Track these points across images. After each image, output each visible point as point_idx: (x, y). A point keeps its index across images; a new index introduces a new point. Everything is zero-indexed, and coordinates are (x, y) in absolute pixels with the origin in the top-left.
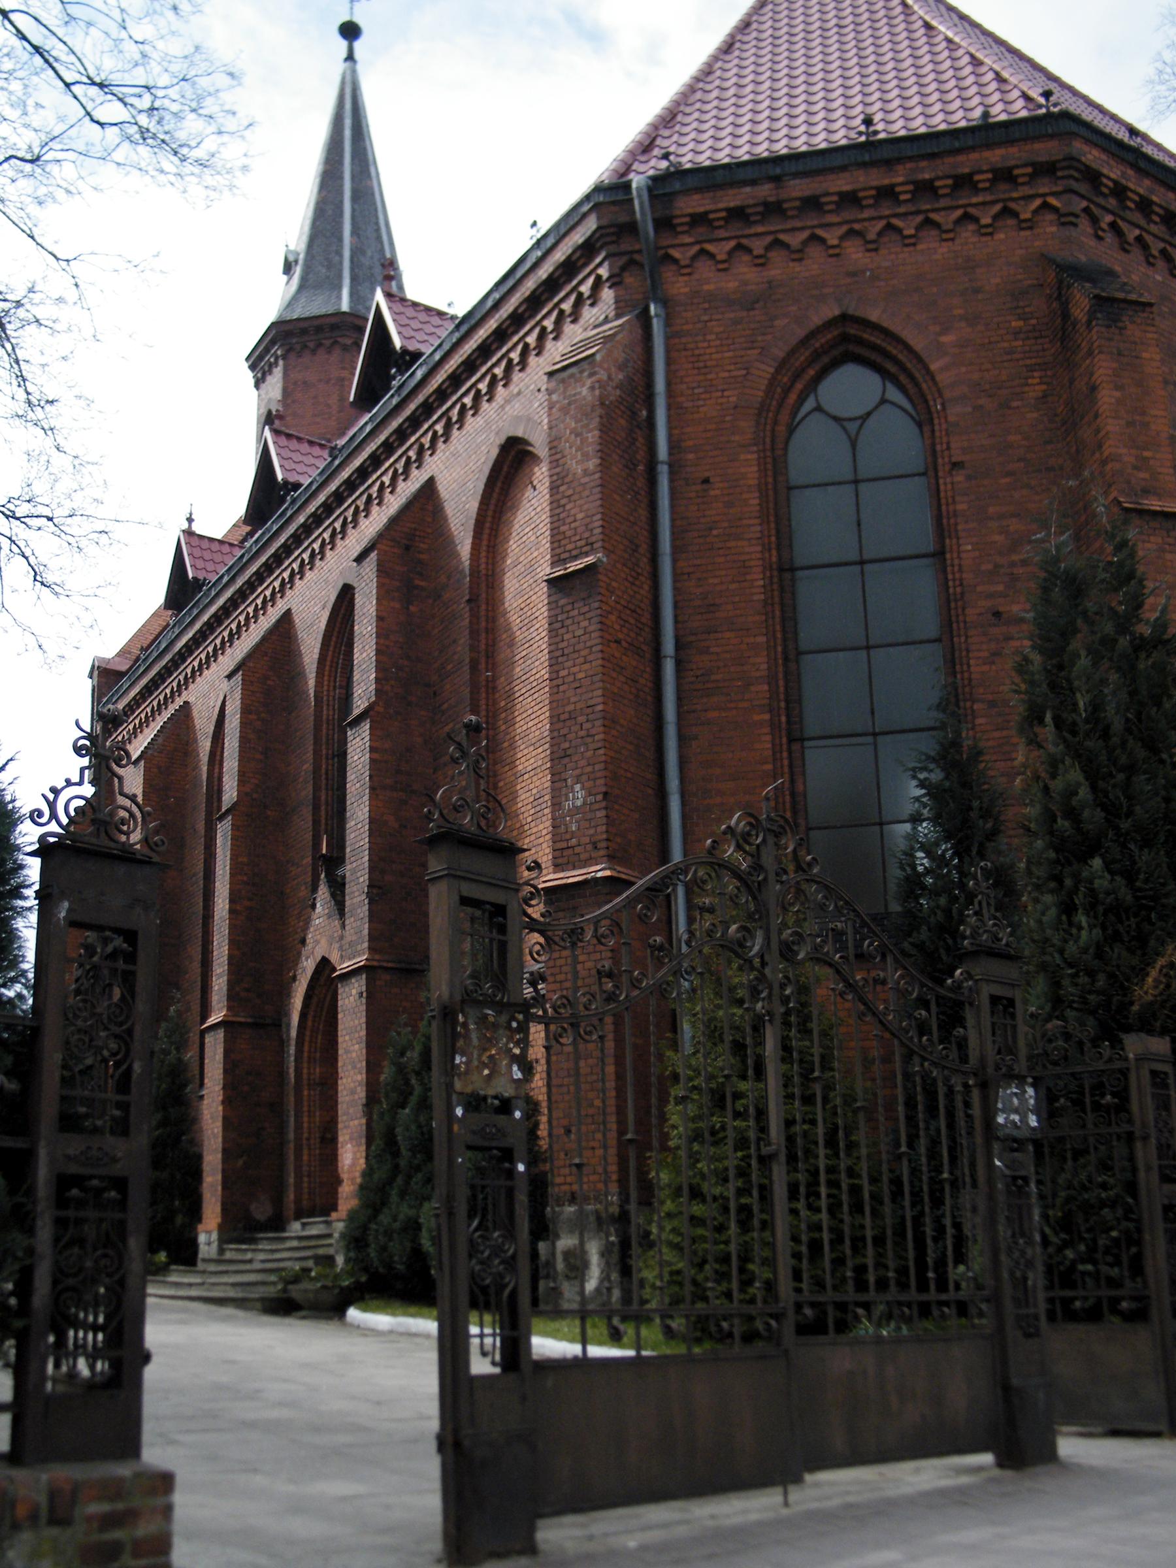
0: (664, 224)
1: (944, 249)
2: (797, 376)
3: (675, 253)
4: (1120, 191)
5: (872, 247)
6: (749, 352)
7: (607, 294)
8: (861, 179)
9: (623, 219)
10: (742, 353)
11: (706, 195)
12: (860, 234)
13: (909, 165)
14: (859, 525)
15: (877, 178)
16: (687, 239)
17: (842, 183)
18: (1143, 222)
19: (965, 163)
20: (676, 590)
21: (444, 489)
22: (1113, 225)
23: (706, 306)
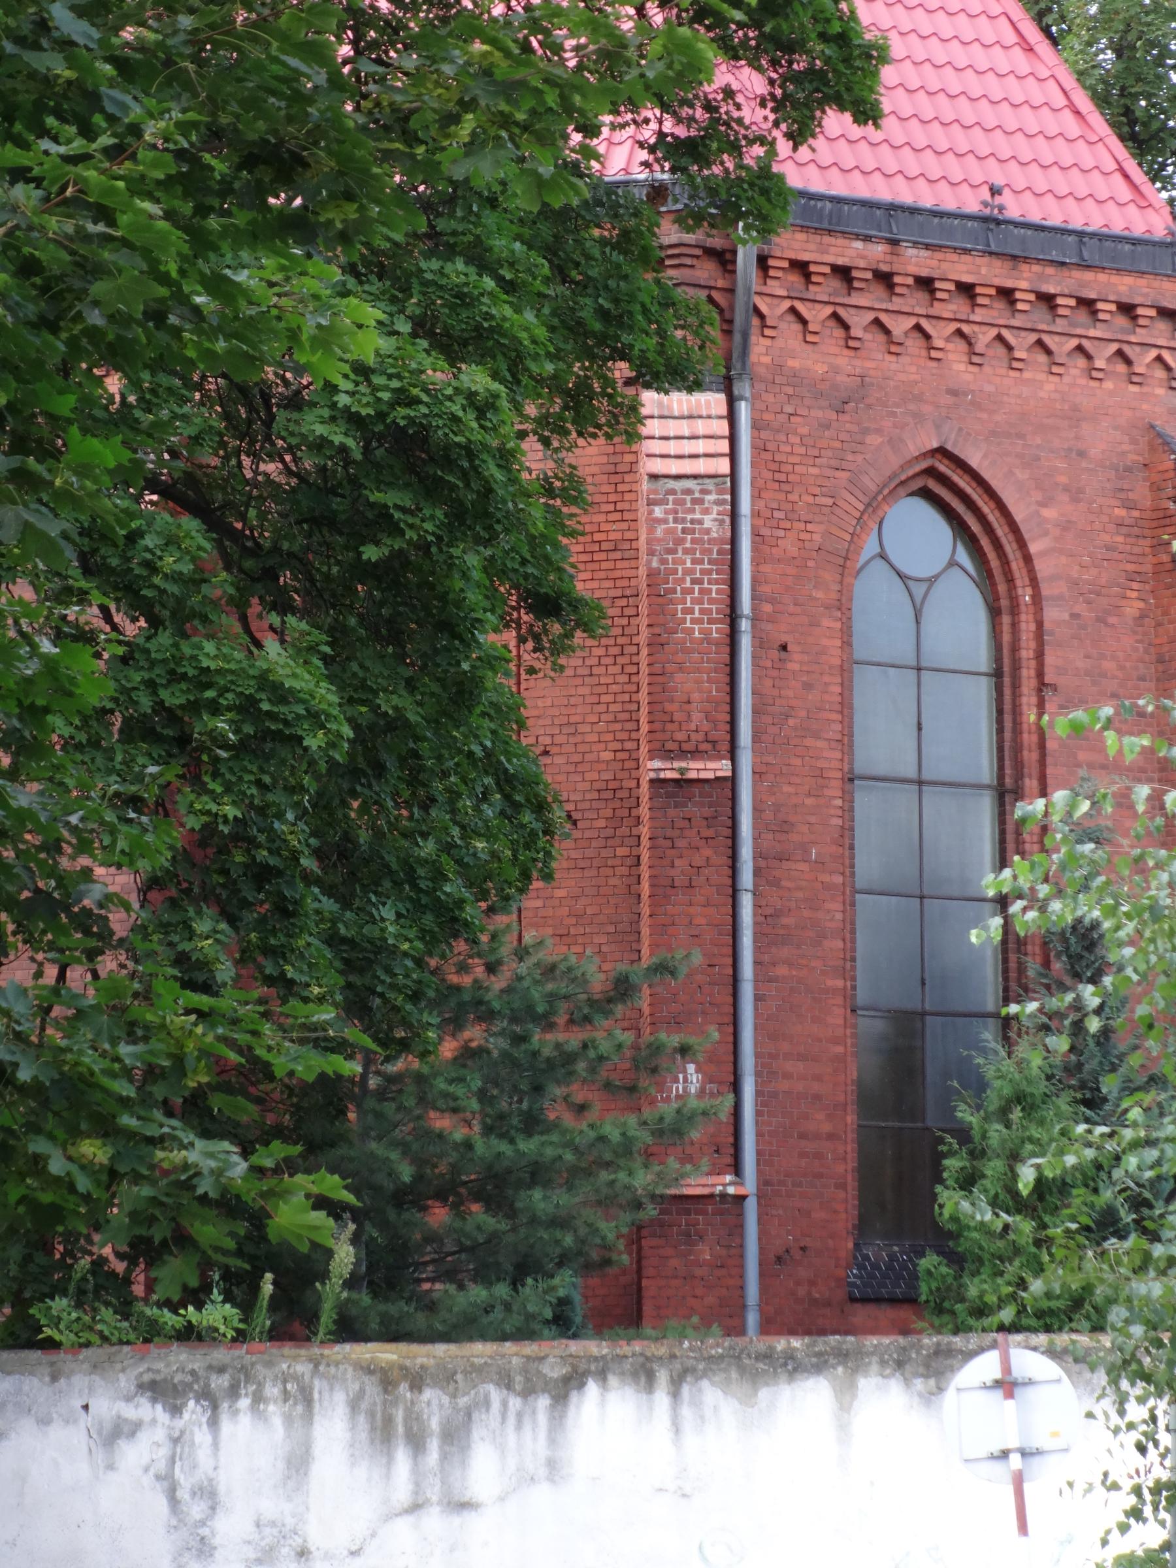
1: (1050, 385)
6: (838, 474)
8: (984, 271)
10: (830, 473)
11: (812, 237)
13: (1036, 268)
14: (920, 728)
19: (1093, 284)
23: (790, 390)
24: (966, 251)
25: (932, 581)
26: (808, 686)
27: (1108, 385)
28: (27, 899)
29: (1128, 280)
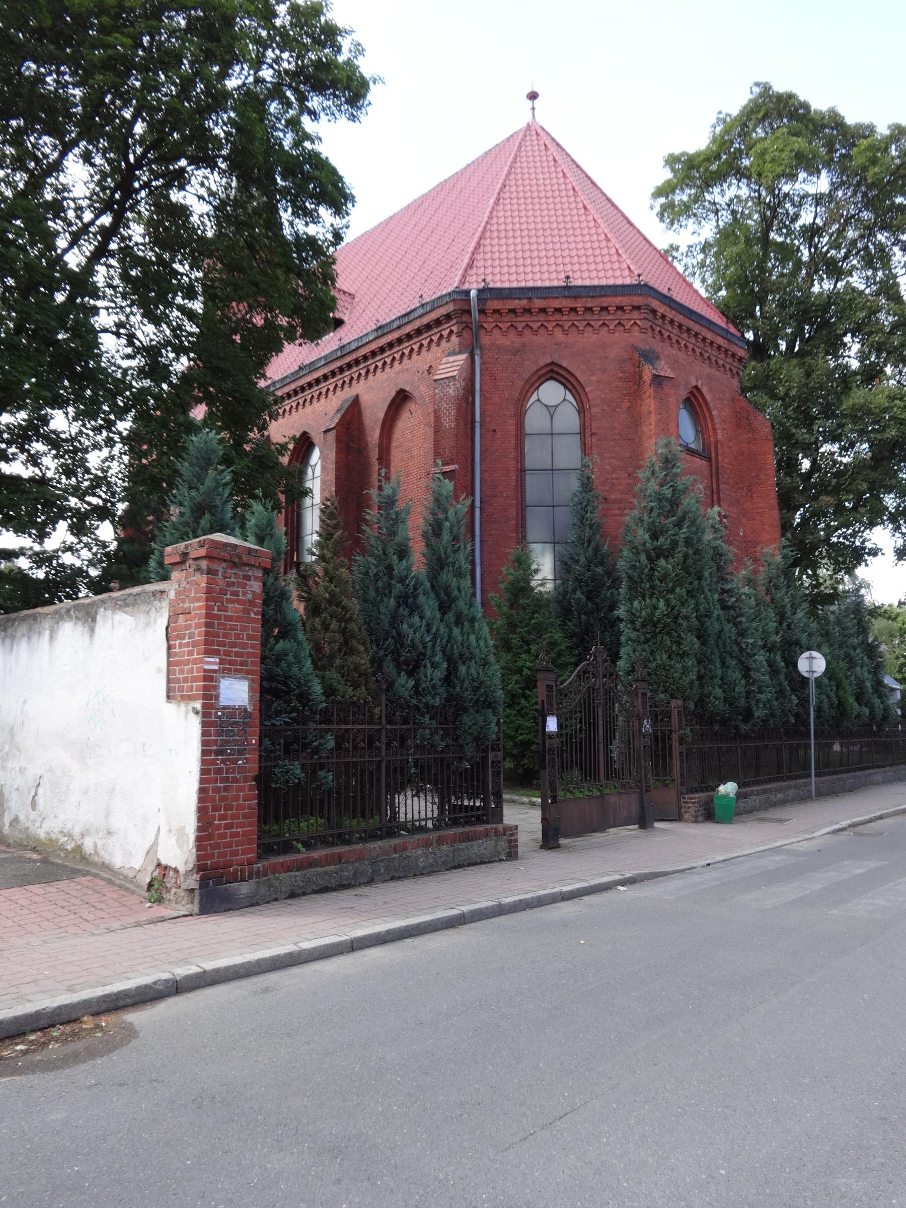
0: (482, 311)
1: (594, 337)
2: (531, 386)
3: (485, 325)
4: (663, 317)
5: (566, 333)
7: (454, 338)
9: (466, 307)
12: (561, 326)
15: (570, 303)
16: (491, 320)
17: (557, 304)
18: (670, 329)
19: (605, 302)
20: (481, 478)
21: (365, 400)
22: (660, 331)
24: (557, 298)
25: (557, 406)
26: (503, 442)
27: (617, 334)
28: (125, 511)
29: (620, 299)
